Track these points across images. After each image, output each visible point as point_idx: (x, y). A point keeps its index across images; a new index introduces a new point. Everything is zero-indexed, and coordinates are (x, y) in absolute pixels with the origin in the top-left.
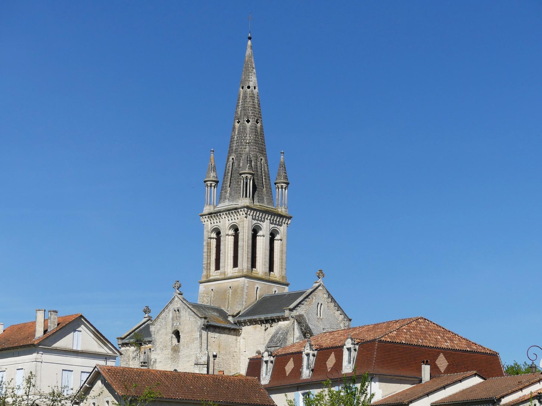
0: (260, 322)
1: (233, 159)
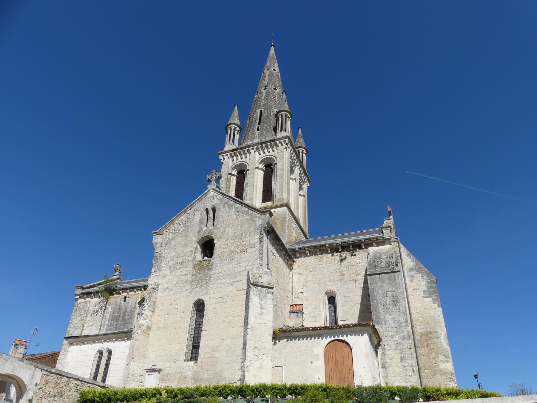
1: (261, 112)
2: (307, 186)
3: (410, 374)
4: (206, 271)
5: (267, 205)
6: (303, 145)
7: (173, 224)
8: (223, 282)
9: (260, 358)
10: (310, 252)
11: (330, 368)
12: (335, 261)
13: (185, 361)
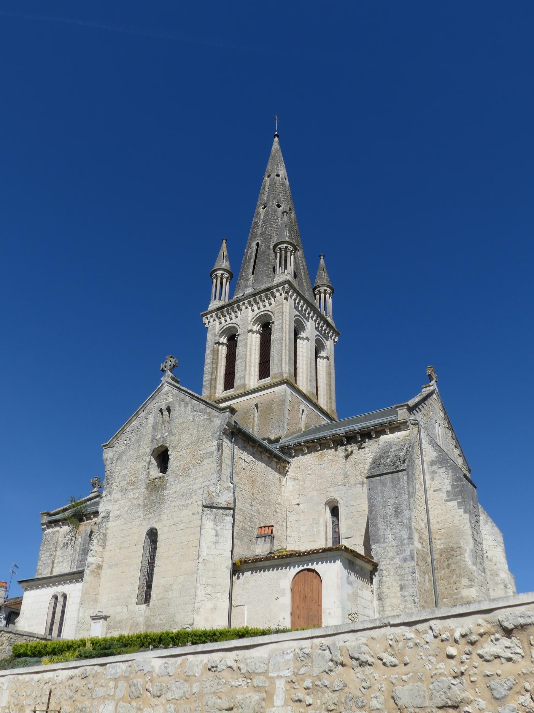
0: (334, 444)
1: (257, 244)
2: (334, 342)
3: (410, 606)
4: (160, 491)
5: (265, 383)
6: (325, 282)
7: (125, 432)
8: (177, 505)
9: (213, 596)
10: (308, 448)
11: (297, 605)
12: (338, 457)
13: (137, 604)
